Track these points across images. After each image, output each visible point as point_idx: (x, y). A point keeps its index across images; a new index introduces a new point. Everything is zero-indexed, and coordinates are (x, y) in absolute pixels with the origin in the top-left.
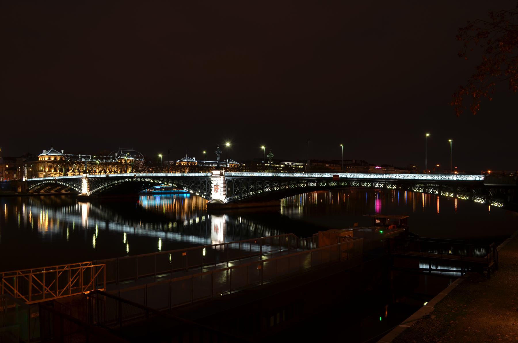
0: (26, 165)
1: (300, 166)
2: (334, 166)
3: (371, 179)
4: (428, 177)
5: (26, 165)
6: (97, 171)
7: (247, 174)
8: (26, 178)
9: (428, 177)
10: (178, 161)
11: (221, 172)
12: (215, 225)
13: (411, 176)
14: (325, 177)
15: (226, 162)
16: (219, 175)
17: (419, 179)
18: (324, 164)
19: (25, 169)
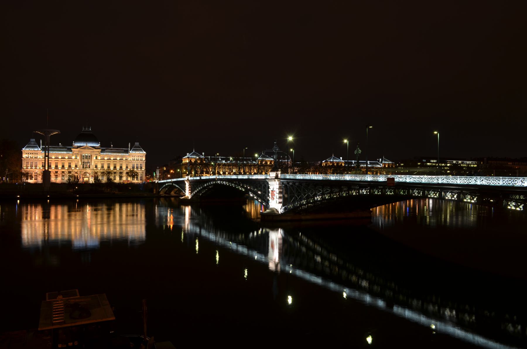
0: (158, 167)
1: (472, 165)
2: (520, 164)
3: (438, 184)
4: (483, 181)
5: (158, 167)
6: (227, 173)
7: (299, 177)
8: (157, 180)
9: (483, 180)
10: (324, 161)
11: (277, 173)
12: (271, 241)
13: (501, 181)
14: (379, 180)
15: (379, 161)
16: (274, 178)
17: (516, 185)
18: (502, 162)
19: (157, 171)
